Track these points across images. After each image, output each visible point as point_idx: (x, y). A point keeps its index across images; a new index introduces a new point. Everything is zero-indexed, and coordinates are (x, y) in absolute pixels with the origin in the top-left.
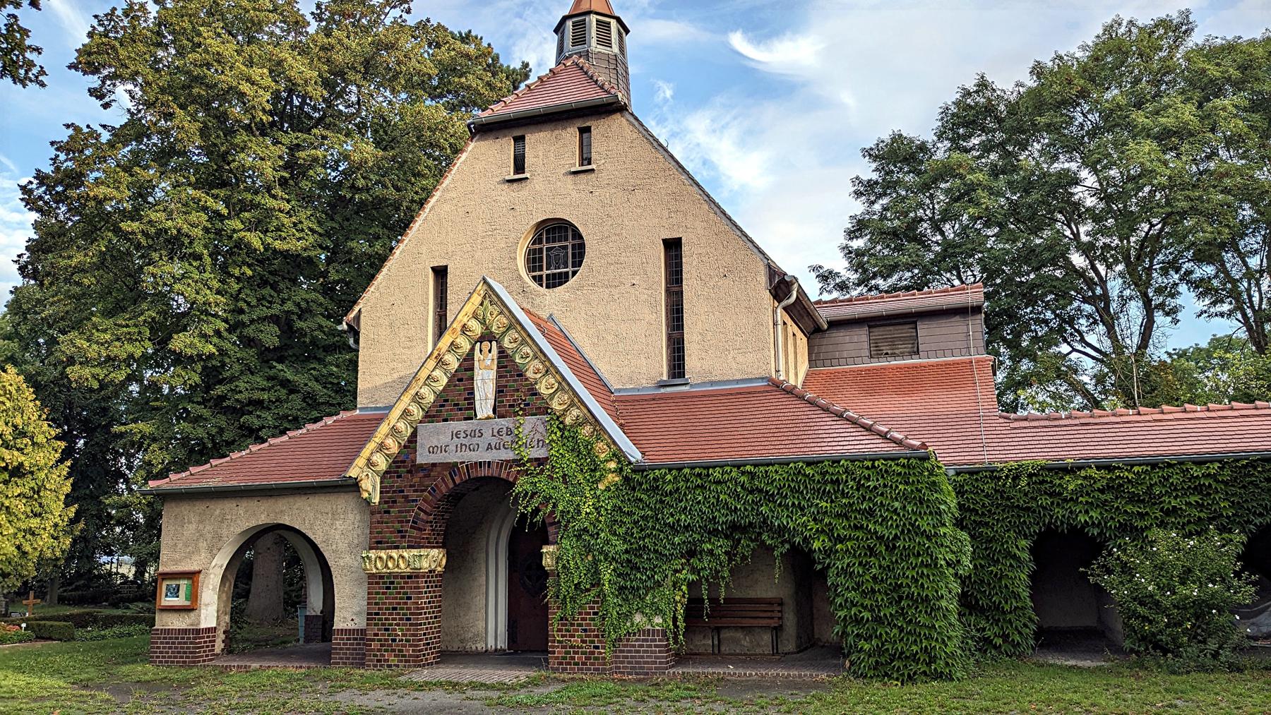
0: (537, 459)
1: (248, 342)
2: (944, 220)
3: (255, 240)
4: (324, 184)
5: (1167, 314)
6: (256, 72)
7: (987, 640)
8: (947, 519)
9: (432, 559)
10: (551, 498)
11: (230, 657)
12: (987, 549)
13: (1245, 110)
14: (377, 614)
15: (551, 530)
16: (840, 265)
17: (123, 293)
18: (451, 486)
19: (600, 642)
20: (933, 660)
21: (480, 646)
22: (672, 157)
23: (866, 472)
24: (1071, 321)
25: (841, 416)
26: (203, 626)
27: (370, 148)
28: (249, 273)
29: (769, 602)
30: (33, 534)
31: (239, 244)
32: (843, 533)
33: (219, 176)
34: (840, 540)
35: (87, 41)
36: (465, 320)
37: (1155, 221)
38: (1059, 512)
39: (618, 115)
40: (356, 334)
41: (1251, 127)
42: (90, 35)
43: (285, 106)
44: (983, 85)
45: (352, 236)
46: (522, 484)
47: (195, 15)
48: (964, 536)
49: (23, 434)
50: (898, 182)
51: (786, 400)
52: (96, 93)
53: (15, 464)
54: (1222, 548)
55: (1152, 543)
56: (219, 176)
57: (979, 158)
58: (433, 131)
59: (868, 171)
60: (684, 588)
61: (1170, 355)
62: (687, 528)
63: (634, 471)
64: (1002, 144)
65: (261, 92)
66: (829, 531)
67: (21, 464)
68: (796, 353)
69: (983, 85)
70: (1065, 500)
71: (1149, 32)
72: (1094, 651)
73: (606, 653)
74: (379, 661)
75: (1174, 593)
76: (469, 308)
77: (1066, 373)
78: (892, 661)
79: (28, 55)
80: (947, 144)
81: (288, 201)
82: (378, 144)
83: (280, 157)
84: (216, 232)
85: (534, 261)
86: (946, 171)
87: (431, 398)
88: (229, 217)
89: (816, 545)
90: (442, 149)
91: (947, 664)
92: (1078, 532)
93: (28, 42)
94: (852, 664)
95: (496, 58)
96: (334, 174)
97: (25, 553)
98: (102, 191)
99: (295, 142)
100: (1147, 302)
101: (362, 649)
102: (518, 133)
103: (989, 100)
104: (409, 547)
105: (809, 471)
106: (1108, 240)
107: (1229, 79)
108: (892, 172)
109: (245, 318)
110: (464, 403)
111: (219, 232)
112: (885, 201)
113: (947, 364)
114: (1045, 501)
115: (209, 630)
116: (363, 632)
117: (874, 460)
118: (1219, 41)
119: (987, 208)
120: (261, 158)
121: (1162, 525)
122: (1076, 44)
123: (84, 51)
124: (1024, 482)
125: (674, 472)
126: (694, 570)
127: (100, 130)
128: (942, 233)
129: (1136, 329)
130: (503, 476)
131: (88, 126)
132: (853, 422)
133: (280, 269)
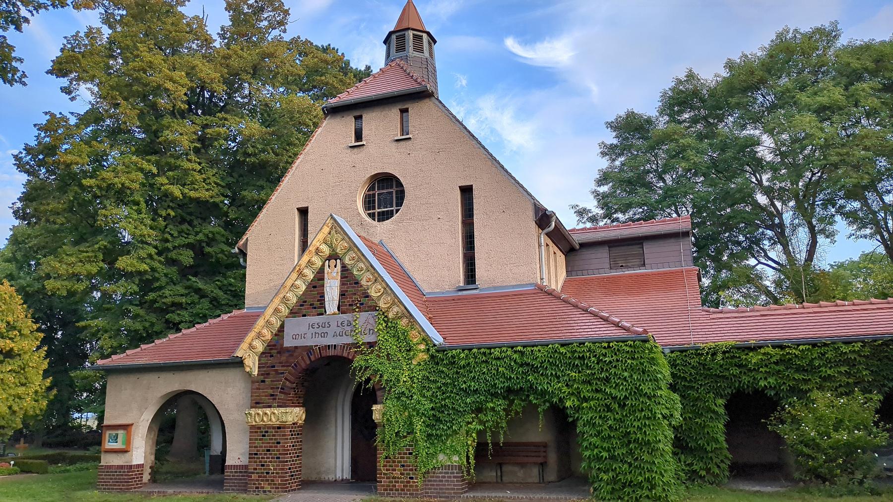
0: (369, 343)
1: (172, 262)
2: (664, 172)
3: (176, 191)
4: (226, 152)
5: (827, 237)
6: (177, 75)
7: (694, 472)
8: (663, 384)
9: (295, 415)
10: (379, 370)
11: (154, 485)
12: (693, 406)
13: (879, 90)
14: (256, 454)
15: (379, 393)
16: (592, 206)
17: (86, 227)
18: (308, 362)
19: (414, 474)
20: (653, 487)
21: (331, 477)
22: (466, 128)
23: (604, 351)
24: (758, 242)
25: (586, 311)
26: (135, 463)
27: (257, 126)
28: (172, 213)
29: (536, 445)
30: (20, 398)
31: (166, 195)
32: (587, 395)
33: (152, 147)
34: (586, 400)
35: (60, 54)
36: (318, 244)
37: (816, 171)
38: (745, 379)
39: (427, 100)
40: (245, 255)
41: (883, 103)
42: (62, 50)
43: (198, 99)
44: (691, 76)
45: (245, 187)
46: (358, 361)
47: (136, 36)
48: (676, 397)
49: (14, 328)
50: (631, 146)
51: (547, 299)
52: (67, 91)
53: (8, 349)
54: (863, 405)
55: (813, 401)
56: (152, 147)
57: (689, 127)
58: (301, 113)
59: (611, 138)
60: (474, 435)
61: (832, 266)
62: (476, 391)
63: (438, 351)
64: (705, 118)
65: (180, 88)
66: (577, 394)
67: (12, 349)
68: (556, 266)
69: (691, 76)
70: (750, 370)
71: (809, 37)
72: (773, 480)
73: (419, 482)
74: (257, 488)
75: (830, 438)
76: (321, 236)
77: (752, 278)
78: (624, 487)
79: (14, 64)
80: (666, 118)
81: (200, 164)
82: (263, 123)
83: (194, 133)
84: (149, 184)
85: (369, 203)
86: (666, 138)
87: (295, 300)
88: (158, 175)
89: (568, 404)
90: (308, 126)
91: (664, 489)
92: (760, 393)
93: (13, 55)
94: (595, 490)
95: (348, 63)
96: (233, 145)
97: (14, 412)
98: (69, 158)
99: (205, 122)
100: (812, 228)
101: (245, 479)
102: (357, 113)
103: (696, 87)
104: (278, 406)
105: (563, 350)
106: (783, 185)
107: (866, 70)
108: (628, 138)
109: (169, 245)
110: (317, 304)
111: (152, 186)
112: (622, 159)
113: (665, 273)
114: (735, 371)
115: (138, 466)
116: (246, 467)
117: (609, 343)
118: (858, 43)
119: (694, 163)
120: (181, 134)
121: (821, 388)
122: (756, 45)
123: (58, 62)
124: (719, 357)
125: (466, 352)
126: (481, 422)
127: (69, 116)
128: (664, 181)
129: (804, 248)
130: (345, 355)
131: (60, 113)
132: (595, 315)
133: (194, 211)
